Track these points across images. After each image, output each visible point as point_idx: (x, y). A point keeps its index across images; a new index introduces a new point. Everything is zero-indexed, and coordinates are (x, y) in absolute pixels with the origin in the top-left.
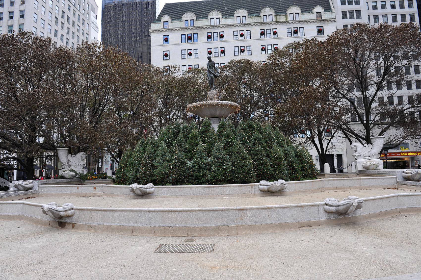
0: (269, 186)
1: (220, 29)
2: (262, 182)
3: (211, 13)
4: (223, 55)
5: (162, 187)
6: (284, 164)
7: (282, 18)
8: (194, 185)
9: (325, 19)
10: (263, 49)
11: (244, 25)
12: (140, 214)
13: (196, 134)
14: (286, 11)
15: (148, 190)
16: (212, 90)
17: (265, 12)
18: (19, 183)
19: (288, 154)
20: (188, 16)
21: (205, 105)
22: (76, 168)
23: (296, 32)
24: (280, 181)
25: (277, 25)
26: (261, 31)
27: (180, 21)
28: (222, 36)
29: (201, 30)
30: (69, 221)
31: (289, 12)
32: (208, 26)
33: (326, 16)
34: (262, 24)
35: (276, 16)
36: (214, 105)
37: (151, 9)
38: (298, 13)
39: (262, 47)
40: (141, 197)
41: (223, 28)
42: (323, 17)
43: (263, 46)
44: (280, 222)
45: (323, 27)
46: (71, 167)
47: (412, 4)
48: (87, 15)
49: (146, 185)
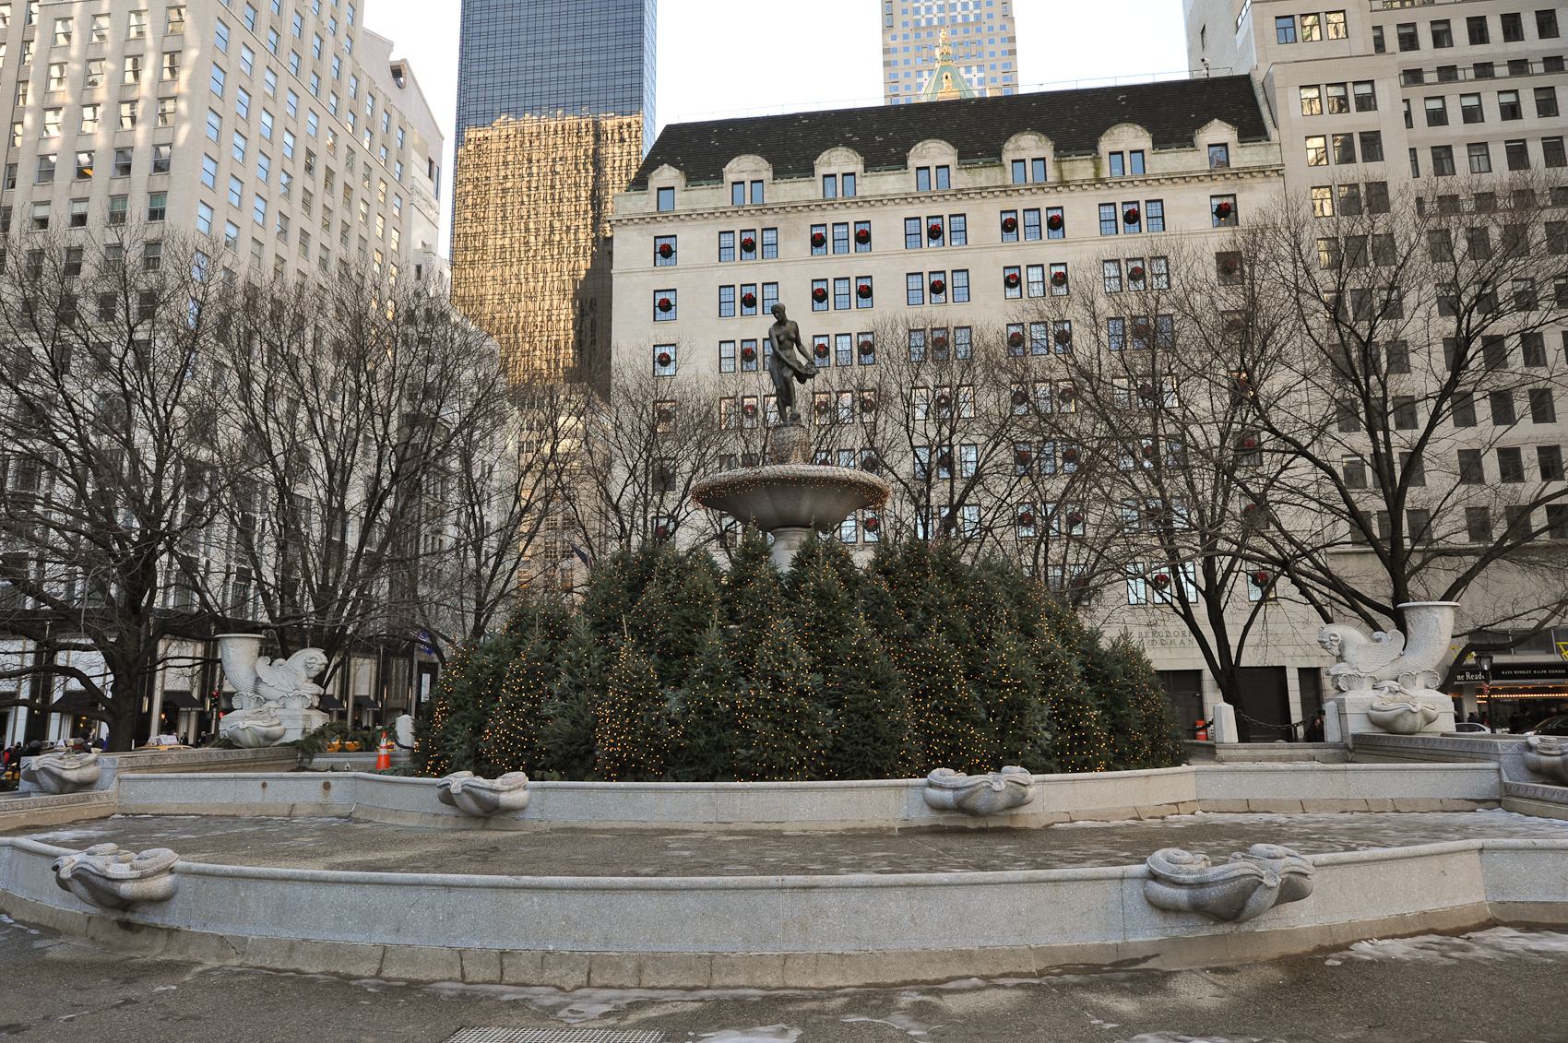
0: (963, 792)
2: (939, 774)
3: (824, 156)
4: (867, 302)
6: (1039, 710)
7: (1081, 168)
10: (1012, 282)
12: (413, 896)
13: (705, 586)
15: (505, 798)
17: (1018, 149)
18: (41, 763)
19: (1053, 670)
20: (744, 167)
21: (755, 480)
23: (1132, 217)
24: (1015, 772)
26: (1005, 217)
28: (863, 238)
30: (157, 921)
31: (1106, 145)
35: (1058, 162)
38: (1142, 151)
40: (479, 825)
42: (1234, 163)
43: (1012, 272)
44: (961, 946)
45: (1234, 196)
46: (268, 704)
48: (398, 166)
49: (499, 780)
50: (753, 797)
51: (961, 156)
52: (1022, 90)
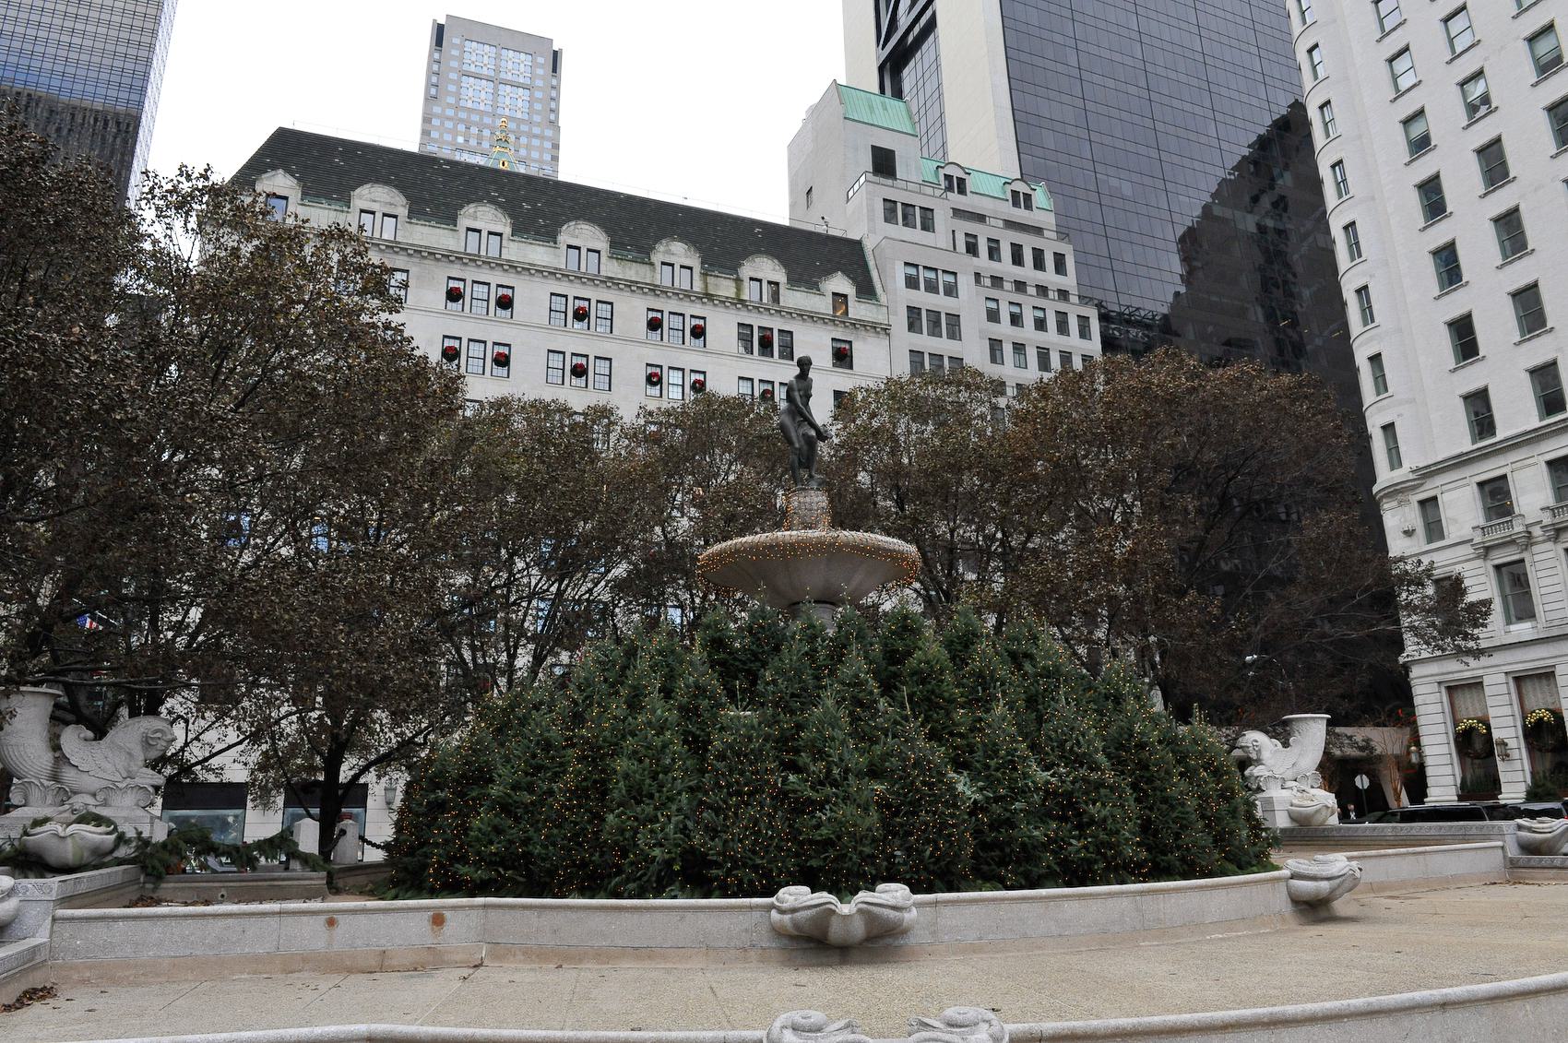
0: (1338, 881)
1: (502, 273)
4: (502, 371)
5: (953, 902)
7: (725, 288)
8: (1012, 888)
9: (860, 320)
10: (654, 380)
11: (592, 280)
14: (741, 265)
16: (812, 489)
17: (669, 252)
22: (105, 804)
25: (707, 307)
27: (338, 208)
29: (426, 262)
31: (747, 270)
32: (455, 252)
33: (863, 313)
34: (655, 290)
35: (705, 275)
36: (869, 552)
37: (115, 138)
39: (650, 370)
41: (512, 275)
45: (850, 343)
47: (1089, 327)
50: (1174, 898)
51: (613, 245)
52: (560, 179)
